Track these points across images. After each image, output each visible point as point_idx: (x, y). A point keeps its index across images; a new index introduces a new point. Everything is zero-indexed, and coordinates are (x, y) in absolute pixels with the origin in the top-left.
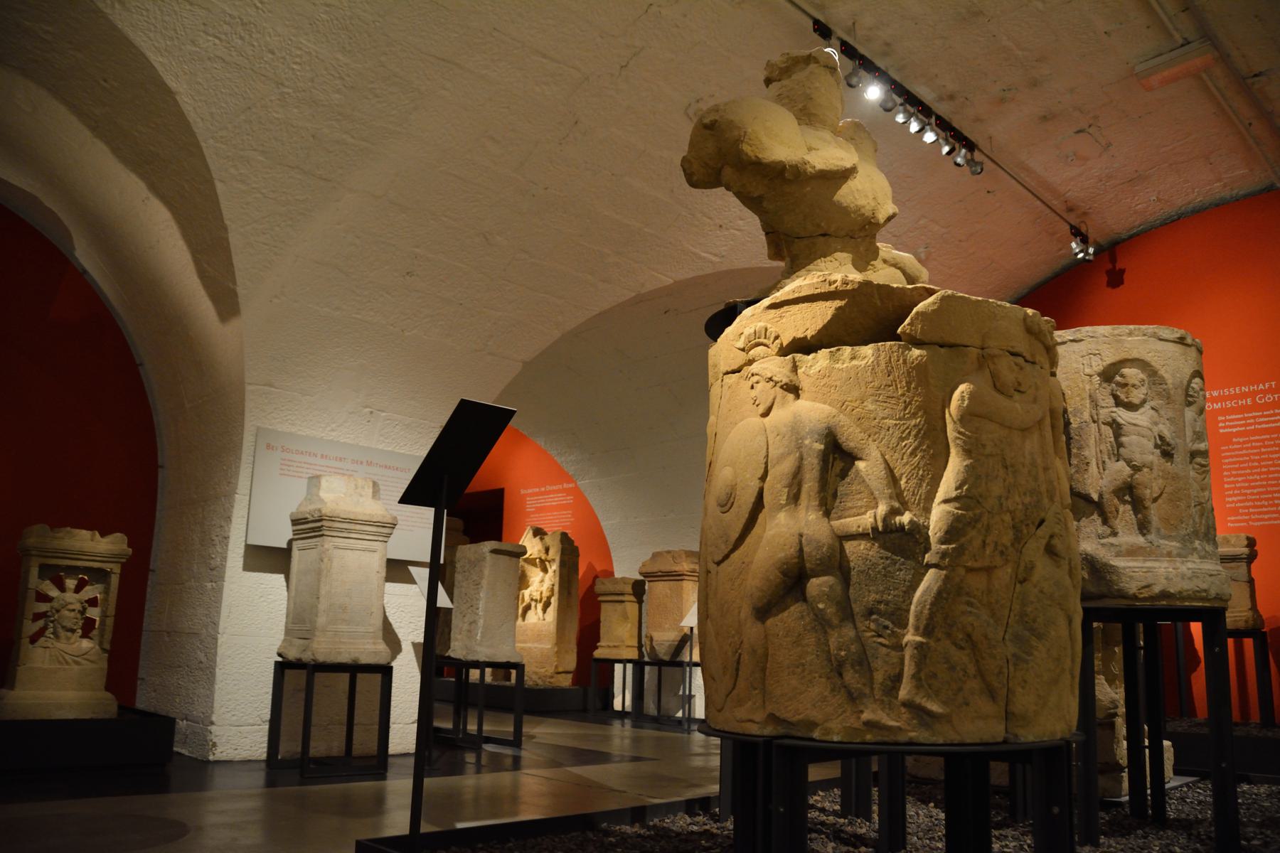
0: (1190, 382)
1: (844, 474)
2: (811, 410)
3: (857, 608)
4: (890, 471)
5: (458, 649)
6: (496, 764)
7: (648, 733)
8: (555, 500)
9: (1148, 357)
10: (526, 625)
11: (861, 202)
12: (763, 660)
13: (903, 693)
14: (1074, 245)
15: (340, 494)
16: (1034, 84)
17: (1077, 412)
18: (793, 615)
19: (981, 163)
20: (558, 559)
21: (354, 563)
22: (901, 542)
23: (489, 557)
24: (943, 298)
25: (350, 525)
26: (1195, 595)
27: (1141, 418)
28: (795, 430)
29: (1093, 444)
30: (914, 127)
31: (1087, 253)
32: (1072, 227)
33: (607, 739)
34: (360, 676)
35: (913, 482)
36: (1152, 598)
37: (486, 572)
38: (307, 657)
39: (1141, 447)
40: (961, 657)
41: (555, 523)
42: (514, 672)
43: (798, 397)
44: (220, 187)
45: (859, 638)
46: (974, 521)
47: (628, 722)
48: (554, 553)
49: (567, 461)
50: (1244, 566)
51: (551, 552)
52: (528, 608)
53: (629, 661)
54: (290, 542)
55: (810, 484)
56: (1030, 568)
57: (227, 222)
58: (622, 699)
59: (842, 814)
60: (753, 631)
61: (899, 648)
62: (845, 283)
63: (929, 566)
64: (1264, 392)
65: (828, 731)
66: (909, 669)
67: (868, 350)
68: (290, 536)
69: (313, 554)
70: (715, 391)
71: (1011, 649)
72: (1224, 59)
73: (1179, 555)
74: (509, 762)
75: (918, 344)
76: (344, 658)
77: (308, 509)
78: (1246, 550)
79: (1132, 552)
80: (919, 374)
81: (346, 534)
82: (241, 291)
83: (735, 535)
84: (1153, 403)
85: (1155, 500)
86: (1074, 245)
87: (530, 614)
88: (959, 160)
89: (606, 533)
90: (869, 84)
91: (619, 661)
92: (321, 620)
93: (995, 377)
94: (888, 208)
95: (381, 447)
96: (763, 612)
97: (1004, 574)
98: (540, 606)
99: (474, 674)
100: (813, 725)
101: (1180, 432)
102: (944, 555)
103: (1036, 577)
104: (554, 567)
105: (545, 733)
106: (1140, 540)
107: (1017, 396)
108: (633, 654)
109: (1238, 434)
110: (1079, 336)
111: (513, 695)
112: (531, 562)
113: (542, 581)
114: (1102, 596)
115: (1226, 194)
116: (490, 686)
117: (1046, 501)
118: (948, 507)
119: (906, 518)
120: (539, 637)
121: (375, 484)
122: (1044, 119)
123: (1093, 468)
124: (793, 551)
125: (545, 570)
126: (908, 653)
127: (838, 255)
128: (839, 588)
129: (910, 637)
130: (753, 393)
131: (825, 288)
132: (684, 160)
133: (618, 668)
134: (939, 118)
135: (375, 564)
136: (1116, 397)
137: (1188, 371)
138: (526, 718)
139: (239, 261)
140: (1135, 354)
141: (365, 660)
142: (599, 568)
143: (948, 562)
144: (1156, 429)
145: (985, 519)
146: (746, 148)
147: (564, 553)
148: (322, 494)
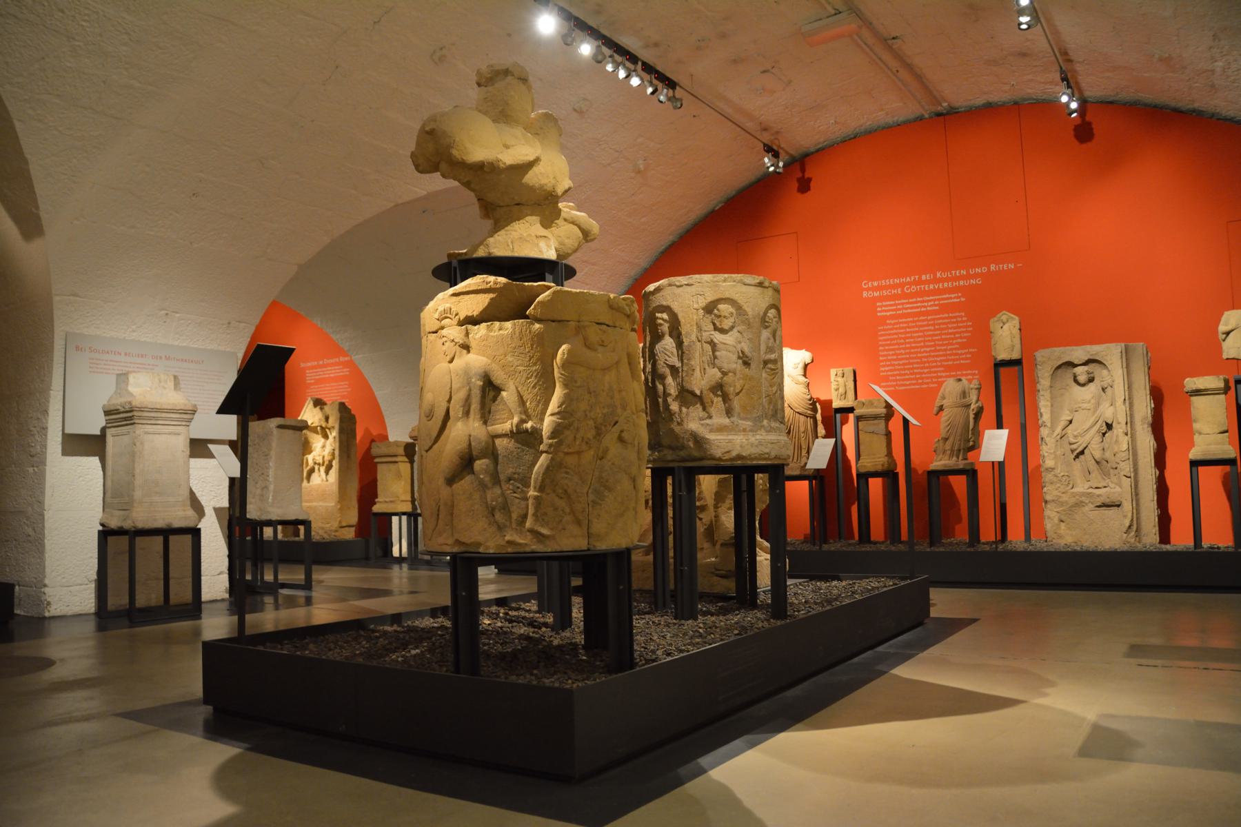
0: (765, 313)
1: (494, 399)
2: (476, 361)
3: (502, 477)
4: (521, 397)
5: (253, 511)
6: (291, 602)
7: (423, 573)
8: (333, 372)
9: (735, 297)
10: (316, 489)
11: (544, 181)
12: (452, 507)
13: (528, 524)
14: (766, 160)
15: (145, 388)
16: (723, 36)
17: (688, 334)
18: (466, 483)
19: (681, 100)
20: (337, 426)
21: (162, 445)
22: (527, 438)
23: (275, 431)
24: (554, 293)
25: (157, 414)
26: (760, 457)
27: (729, 339)
28: (467, 373)
29: (698, 357)
30: (622, 74)
31: (777, 167)
32: (765, 145)
33: (388, 580)
34: (172, 538)
35: (534, 404)
36: (731, 459)
37: (274, 445)
38: (127, 525)
39: (728, 359)
40: (561, 503)
41: (334, 393)
42: (302, 528)
43: (469, 352)
44: (18, 125)
45: (503, 494)
46: (568, 427)
47: (405, 566)
48: (334, 421)
49: (340, 338)
50: (882, 422)
51: (331, 420)
52: (312, 471)
53: (404, 514)
54: (103, 430)
55: (475, 406)
56: (606, 451)
57: (28, 156)
58: (399, 547)
59: (538, 612)
60: (445, 492)
61: (526, 499)
62: (496, 283)
63: (542, 452)
64: (910, 284)
65: (487, 548)
66: (531, 511)
67: (509, 324)
68: (103, 424)
69: (126, 439)
70: (424, 341)
71: (592, 497)
72: (868, 24)
73: (751, 431)
74: (302, 601)
75: (539, 321)
76: (160, 524)
77: (118, 402)
78: (884, 411)
79: (721, 429)
80: (539, 339)
81: (154, 421)
82: (42, 214)
83: (435, 434)
84: (739, 328)
85: (738, 394)
86: (766, 160)
87: (315, 476)
88: (662, 98)
89: (380, 402)
90: (582, 42)
91: (396, 514)
92: (138, 494)
93: (585, 339)
94: (567, 183)
95: (176, 343)
96: (450, 481)
97: (589, 455)
98: (323, 469)
99: (268, 532)
100: (479, 544)
101: (757, 348)
102: (550, 446)
103: (610, 455)
104: (334, 434)
105: (329, 577)
106: (726, 421)
107: (600, 349)
108: (407, 508)
109: (891, 317)
110: (691, 282)
111: (305, 549)
112: (314, 430)
113: (324, 447)
114: (701, 459)
115: (890, 120)
116: (281, 542)
117: (619, 411)
118: (554, 418)
119: (529, 425)
120: (323, 496)
121: (175, 377)
122: (735, 62)
123: (697, 373)
124: (465, 445)
125: (326, 437)
126: (531, 502)
127: (528, 218)
128: (492, 467)
129: (532, 493)
130: (444, 348)
131: (484, 286)
132: (413, 155)
133: (395, 519)
134: (644, 64)
135: (180, 444)
136: (714, 324)
137: (764, 305)
138: (314, 567)
139: (39, 188)
140: (727, 295)
141: (177, 524)
142: (375, 433)
143: (554, 449)
144: (739, 347)
145: (575, 425)
146: (454, 152)
147: (342, 420)
148: (130, 388)
